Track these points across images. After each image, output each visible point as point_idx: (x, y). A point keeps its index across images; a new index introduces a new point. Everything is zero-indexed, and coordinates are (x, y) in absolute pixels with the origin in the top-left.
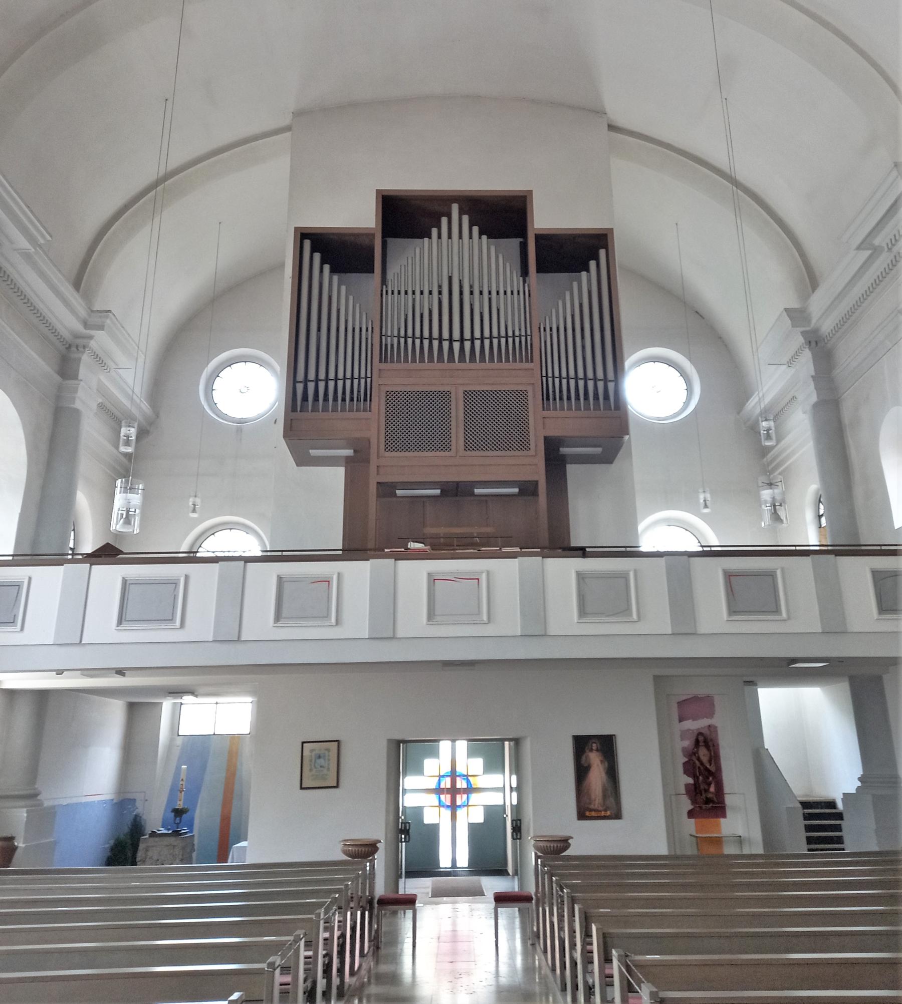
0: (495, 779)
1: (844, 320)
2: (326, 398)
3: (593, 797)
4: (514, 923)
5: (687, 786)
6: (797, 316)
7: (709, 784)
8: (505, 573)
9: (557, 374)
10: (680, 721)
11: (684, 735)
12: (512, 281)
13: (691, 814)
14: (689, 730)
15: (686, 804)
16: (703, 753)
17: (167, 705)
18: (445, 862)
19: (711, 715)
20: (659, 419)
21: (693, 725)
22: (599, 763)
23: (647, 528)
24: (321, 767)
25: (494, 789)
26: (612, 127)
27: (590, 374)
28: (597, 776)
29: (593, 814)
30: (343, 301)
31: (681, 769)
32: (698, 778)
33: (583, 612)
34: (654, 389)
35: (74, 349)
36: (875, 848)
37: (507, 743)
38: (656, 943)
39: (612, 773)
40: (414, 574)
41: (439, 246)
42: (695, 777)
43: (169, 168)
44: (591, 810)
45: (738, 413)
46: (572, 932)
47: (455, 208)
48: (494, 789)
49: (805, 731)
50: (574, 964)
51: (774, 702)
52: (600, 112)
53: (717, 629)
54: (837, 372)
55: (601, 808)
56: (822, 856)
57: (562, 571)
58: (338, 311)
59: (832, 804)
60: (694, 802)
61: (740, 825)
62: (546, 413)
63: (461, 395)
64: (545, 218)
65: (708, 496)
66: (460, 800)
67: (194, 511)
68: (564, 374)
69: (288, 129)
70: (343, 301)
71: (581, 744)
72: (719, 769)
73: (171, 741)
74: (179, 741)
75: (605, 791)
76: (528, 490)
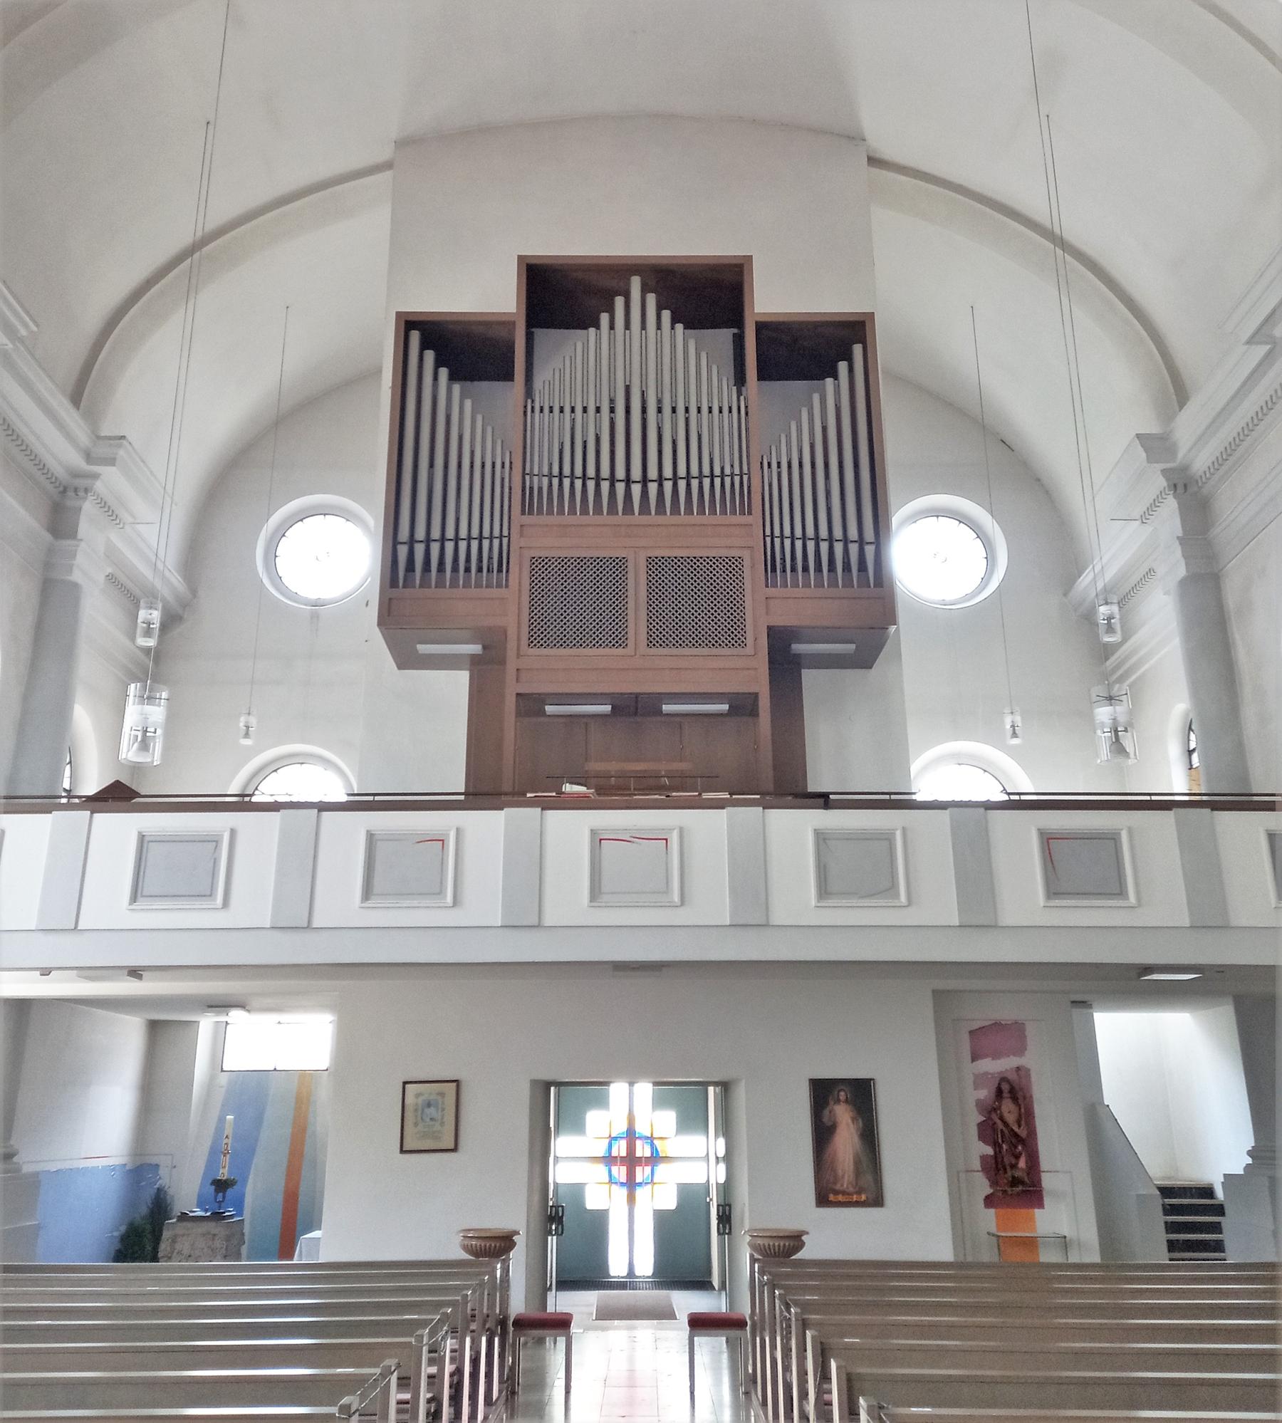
3: (840, 1173)
5: (984, 1158)
6: (1156, 446)
10: (973, 1060)
11: (979, 1080)
13: (989, 1201)
14: (986, 1073)
15: (983, 1187)
16: (1009, 1110)
18: (617, 1268)
19: (1020, 1050)
23: (925, 768)
26: (874, 161)
28: (846, 1141)
29: (840, 1198)
31: (973, 1131)
32: (1001, 1147)
33: (824, 891)
34: (937, 555)
35: (71, 493)
39: (869, 1136)
40: (569, 831)
42: (996, 1145)
44: (836, 1193)
45: (1065, 595)
46: (803, 1374)
47: (636, 283)
51: (1119, 1033)
52: (855, 138)
53: (1030, 917)
55: (851, 1189)
59: (1208, 1192)
60: (994, 1183)
64: (770, 298)
66: (641, 1173)
67: (247, 735)
69: (388, 166)
71: (822, 1091)
72: (1032, 1133)
74: (223, 1079)
75: (857, 1163)
76: (743, 706)
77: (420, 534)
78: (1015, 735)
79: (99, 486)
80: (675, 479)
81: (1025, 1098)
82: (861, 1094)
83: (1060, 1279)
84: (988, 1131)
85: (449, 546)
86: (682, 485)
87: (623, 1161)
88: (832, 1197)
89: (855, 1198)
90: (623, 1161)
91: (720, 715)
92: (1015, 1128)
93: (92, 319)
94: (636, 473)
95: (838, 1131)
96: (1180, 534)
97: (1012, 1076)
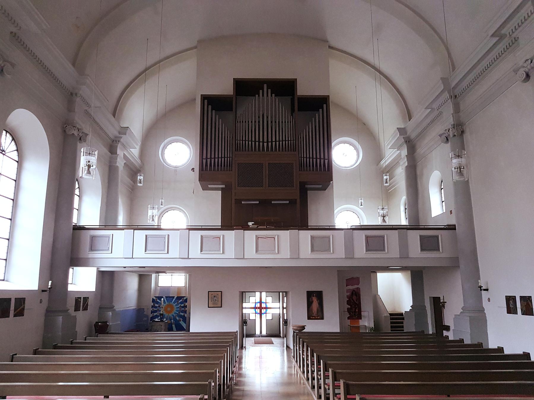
0: (277, 305)
1: (420, 134)
2: (214, 166)
4: (283, 353)
5: (348, 309)
6: (402, 131)
7: (356, 309)
8: (285, 235)
9: (305, 156)
12: (288, 117)
13: (349, 318)
16: (354, 297)
17: (154, 276)
18: (258, 332)
20: (345, 167)
21: (351, 287)
23: (336, 145)
24: (215, 300)
25: (275, 308)
26: (331, 47)
27: (318, 157)
28: (315, 305)
30: (220, 126)
33: (312, 250)
34: (344, 154)
35: (115, 142)
36: (414, 331)
37: (281, 293)
38: (334, 359)
40: (250, 236)
41: (259, 101)
43: (147, 66)
45: (377, 165)
46: (307, 356)
47: (265, 86)
48: (275, 308)
49: (394, 290)
50: (308, 365)
51: (382, 278)
52: (326, 41)
53: (361, 254)
54: (415, 154)
56: (399, 333)
57: (305, 236)
58: (219, 128)
59: (402, 314)
61: (367, 322)
62: (301, 172)
63: (267, 165)
64: (302, 90)
65: (362, 201)
66: (263, 311)
67: (162, 205)
68: (308, 156)
69: (195, 47)
70: (220, 126)
71: (310, 294)
73: (156, 288)
74: (159, 288)
75: (317, 310)
76: (293, 202)
77: (209, 156)
78: (361, 205)
79: (122, 140)
80: (276, 141)
82: (319, 295)
83: (365, 336)
84: (348, 303)
85: (216, 160)
86: (278, 143)
87: (259, 308)
90: (259, 308)
91: (287, 203)
93: (117, 94)
94: (265, 140)
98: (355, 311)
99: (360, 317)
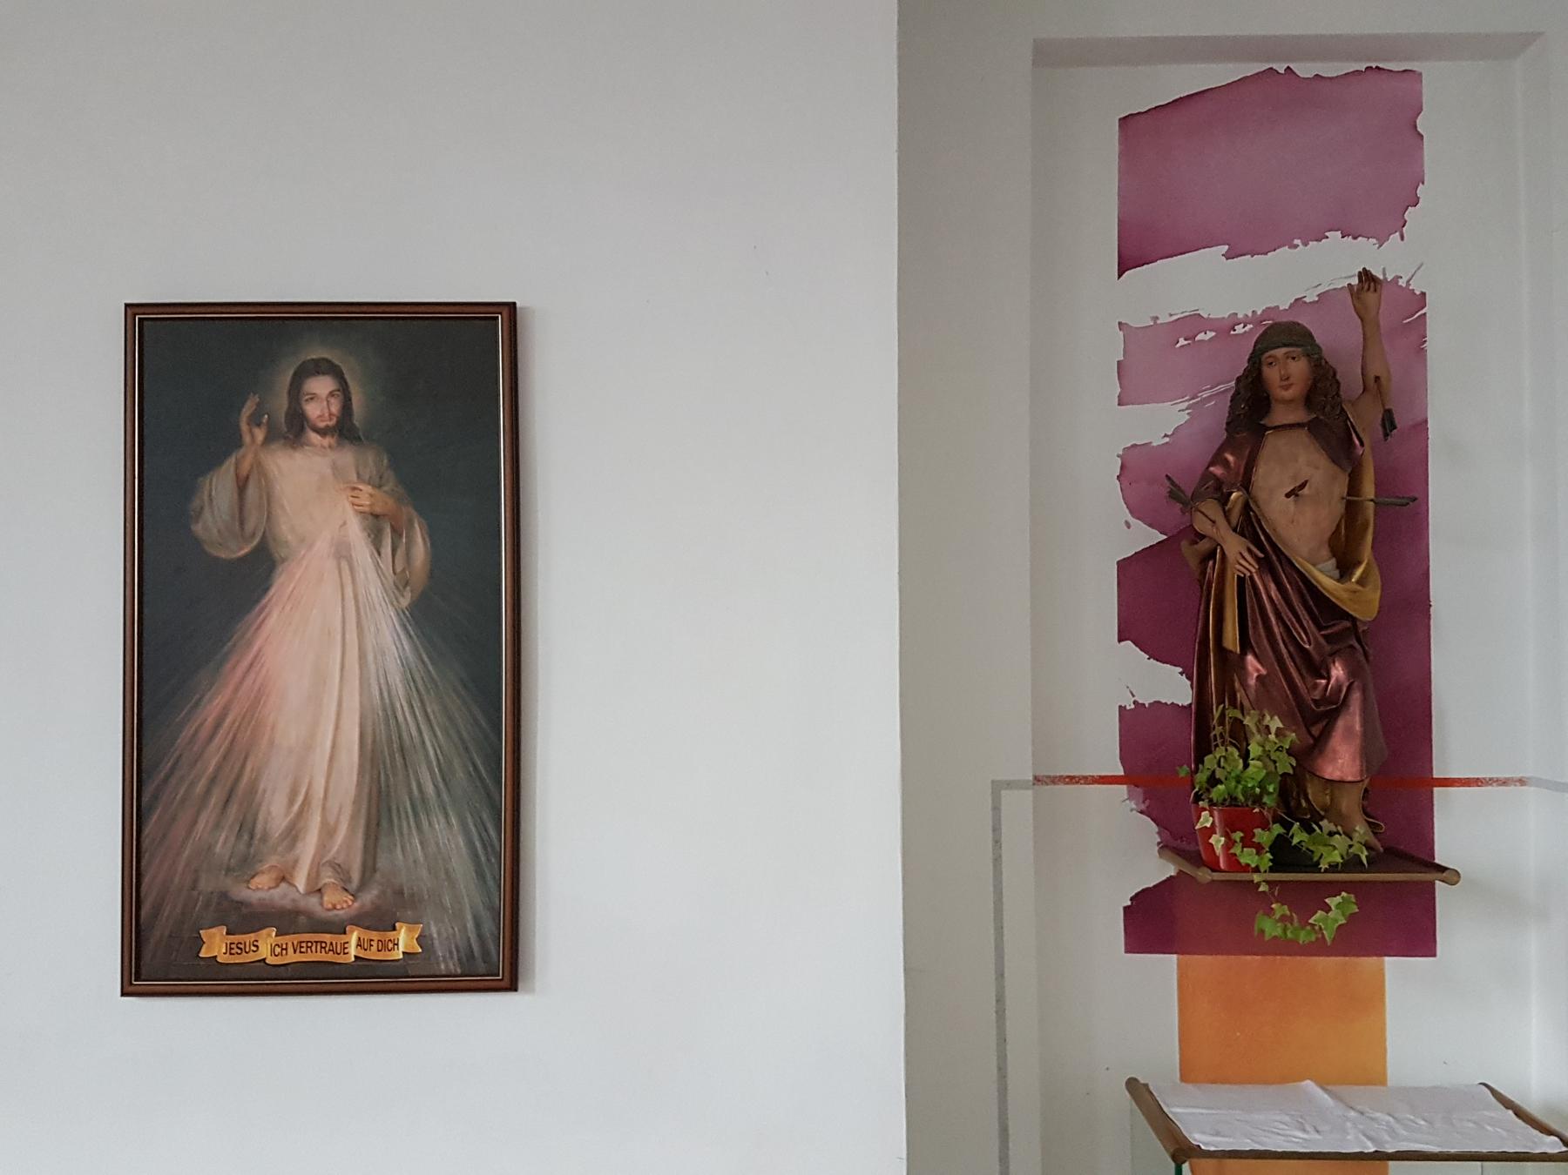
3: (276, 813)
5: (1138, 725)
7: (1317, 720)
10: (1125, 265)
11: (1143, 365)
13: (1151, 922)
14: (1192, 323)
15: (1127, 853)
16: (1296, 492)
19: (1386, 202)
21: (1225, 288)
22: (356, 532)
28: (329, 643)
29: (267, 946)
31: (1101, 601)
32: (1230, 665)
39: (473, 628)
42: (1212, 667)
44: (246, 919)
55: (336, 902)
60: (1179, 841)
71: (200, 376)
72: (1410, 605)
75: (384, 764)
81: (1388, 422)
82: (441, 394)
84: (1160, 603)
88: (216, 944)
89: (353, 944)
92: (1325, 578)
95: (284, 585)
96: (1164, 319)
97: (1338, 337)
98: (1296, 798)
99: (1397, 897)
